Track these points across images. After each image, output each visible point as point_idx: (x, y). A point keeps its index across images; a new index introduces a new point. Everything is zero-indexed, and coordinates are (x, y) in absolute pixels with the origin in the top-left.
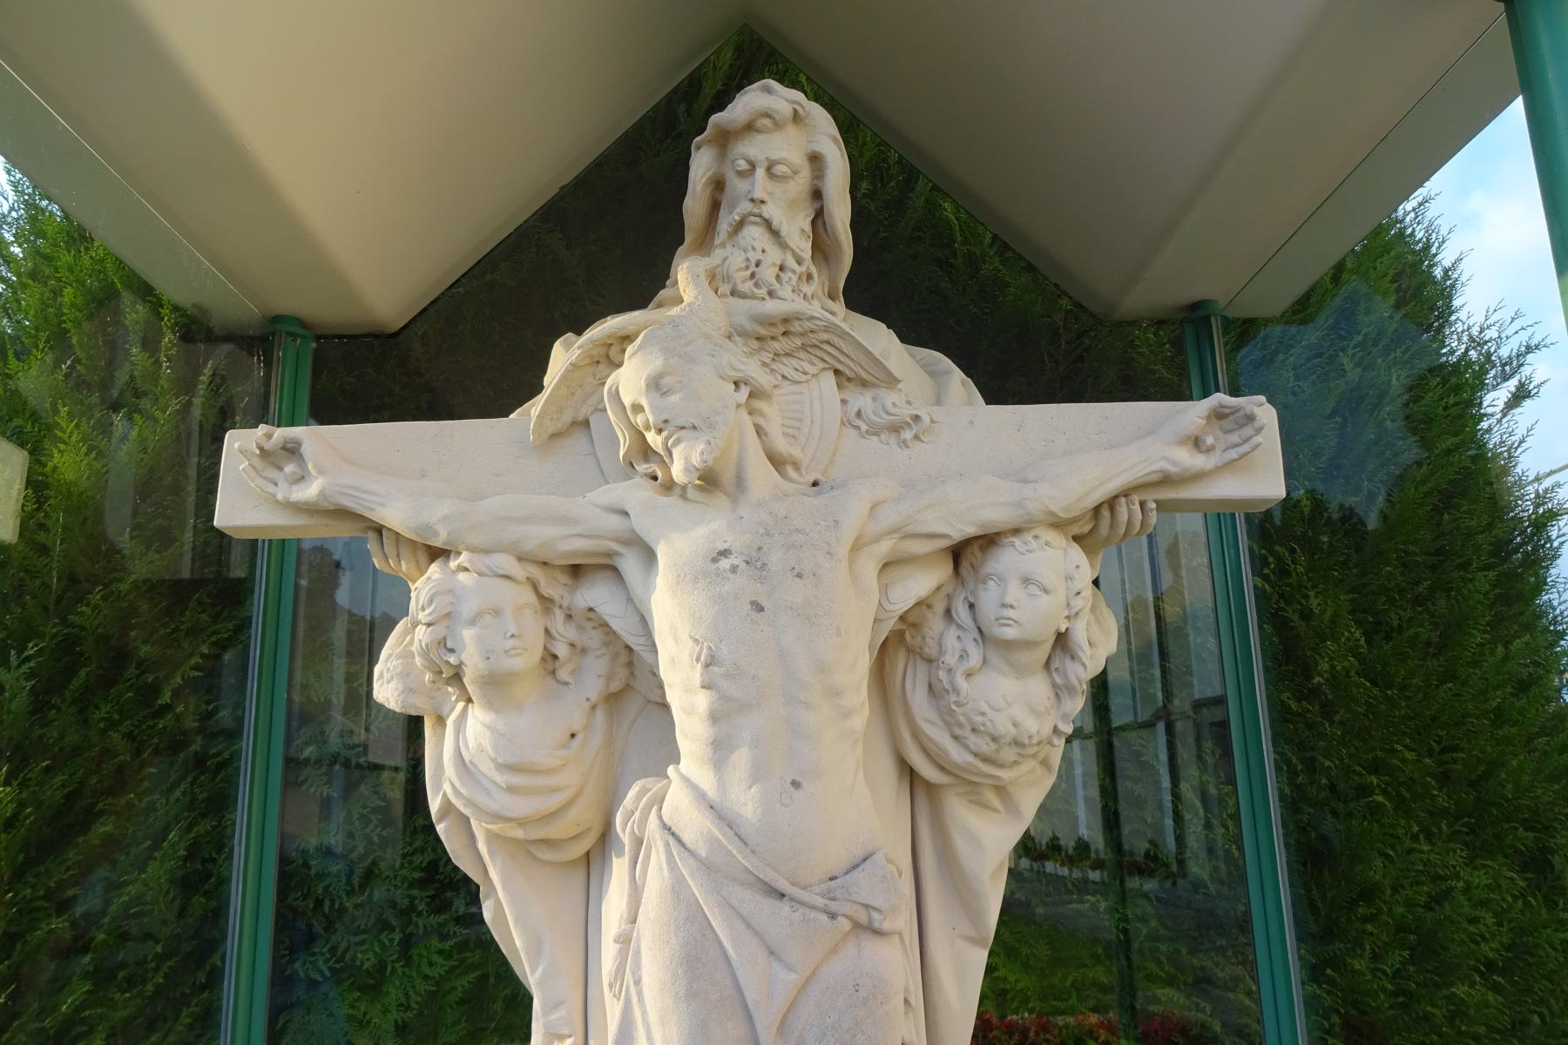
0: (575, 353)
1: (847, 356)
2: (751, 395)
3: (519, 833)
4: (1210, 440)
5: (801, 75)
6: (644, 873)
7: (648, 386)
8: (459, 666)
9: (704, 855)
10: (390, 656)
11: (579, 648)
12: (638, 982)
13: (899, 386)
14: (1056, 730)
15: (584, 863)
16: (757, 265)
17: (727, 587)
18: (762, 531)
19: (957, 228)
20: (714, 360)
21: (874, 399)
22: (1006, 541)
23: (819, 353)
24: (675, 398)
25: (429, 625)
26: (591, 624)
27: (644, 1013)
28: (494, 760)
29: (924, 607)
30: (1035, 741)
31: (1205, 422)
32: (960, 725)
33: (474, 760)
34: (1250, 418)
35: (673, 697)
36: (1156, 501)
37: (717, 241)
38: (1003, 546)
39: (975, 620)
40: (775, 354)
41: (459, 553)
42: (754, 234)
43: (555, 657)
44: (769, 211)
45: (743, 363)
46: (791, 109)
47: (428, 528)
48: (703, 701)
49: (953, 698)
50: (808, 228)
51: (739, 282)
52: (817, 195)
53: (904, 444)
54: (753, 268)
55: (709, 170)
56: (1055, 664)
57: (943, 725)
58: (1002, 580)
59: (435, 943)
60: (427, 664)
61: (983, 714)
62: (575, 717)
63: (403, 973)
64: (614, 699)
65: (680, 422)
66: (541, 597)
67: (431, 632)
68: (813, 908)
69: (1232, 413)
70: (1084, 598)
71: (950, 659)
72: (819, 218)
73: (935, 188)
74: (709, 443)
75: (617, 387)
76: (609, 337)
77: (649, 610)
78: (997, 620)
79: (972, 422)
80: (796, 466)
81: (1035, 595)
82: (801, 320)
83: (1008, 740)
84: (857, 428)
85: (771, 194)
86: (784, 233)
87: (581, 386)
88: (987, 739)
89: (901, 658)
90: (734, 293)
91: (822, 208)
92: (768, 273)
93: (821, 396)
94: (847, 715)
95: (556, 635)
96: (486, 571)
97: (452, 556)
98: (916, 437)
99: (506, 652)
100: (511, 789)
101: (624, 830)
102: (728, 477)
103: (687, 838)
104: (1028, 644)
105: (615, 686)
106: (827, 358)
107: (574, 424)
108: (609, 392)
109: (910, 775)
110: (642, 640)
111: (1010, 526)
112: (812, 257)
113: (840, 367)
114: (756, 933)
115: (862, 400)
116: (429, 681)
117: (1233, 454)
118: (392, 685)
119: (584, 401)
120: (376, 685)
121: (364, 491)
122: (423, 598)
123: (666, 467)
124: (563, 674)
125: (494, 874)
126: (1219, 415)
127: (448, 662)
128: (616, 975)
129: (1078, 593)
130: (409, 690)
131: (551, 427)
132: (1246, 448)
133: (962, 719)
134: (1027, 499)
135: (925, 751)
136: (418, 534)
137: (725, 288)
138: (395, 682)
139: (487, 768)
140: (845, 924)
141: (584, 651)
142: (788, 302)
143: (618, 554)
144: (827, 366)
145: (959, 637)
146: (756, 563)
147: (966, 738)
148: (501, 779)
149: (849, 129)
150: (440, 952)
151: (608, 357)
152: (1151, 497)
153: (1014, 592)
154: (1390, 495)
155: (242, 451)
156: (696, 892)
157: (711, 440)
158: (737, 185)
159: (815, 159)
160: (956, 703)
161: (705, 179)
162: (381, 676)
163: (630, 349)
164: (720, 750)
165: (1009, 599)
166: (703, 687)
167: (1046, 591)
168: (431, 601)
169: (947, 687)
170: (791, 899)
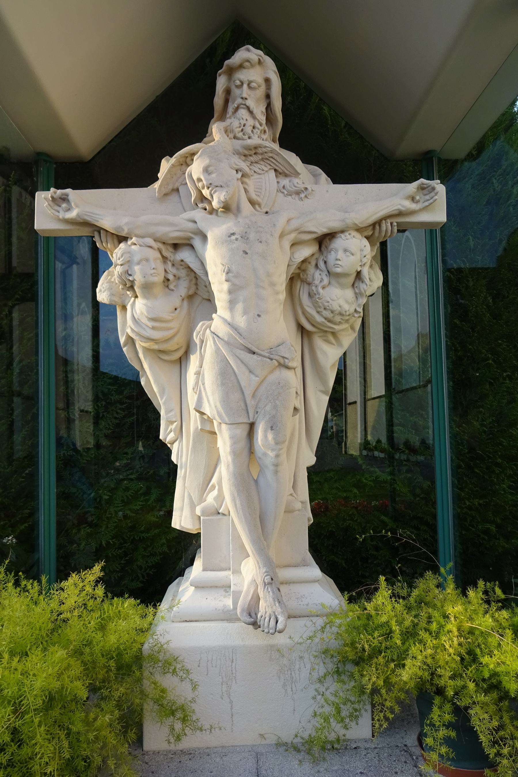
0: (170, 164)
1: (279, 163)
2: (242, 176)
3: (156, 347)
4: (418, 198)
5: (262, 44)
6: (205, 351)
7: (203, 171)
8: (133, 282)
9: (226, 340)
10: (103, 283)
11: (177, 277)
12: (203, 384)
13: (300, 176)
14: (356, 311)
15: (179, 360)
16: (244, 126)
17: (234, 245)
18: (247, 226)
19: (329, 118)
20: (228, 161)
21: (290, 181)
22: (339, 235)
23: (268, 162)
24: (214, 175)
25: (121, 265)
26: (182, 267)
27: (206, 393)
28: (147, 317)
29: (308, 263)
30: (348, 313)
31: (416, 190)
32: (320, 307)
33: (139, 318)
34: (434, 189)
35: (215, 288)
36: (397, 223)
37: (228, 116)
38: (337, 238)
39: (326, 268)
40: (251, 162)
41: (132, 238)
42: (243, 113)
43: (168, 280)
44: (249, 103)
45: (239, 162)
46: (257, 59)
47: (120, 228)
48: (226, 286)
49: (317, 296)
50: (264, 111)
51: (237, 133)
52: (268, 96)
53: (301, 199)
54: (242, 127)
55: (224, 85)
56: (356, 285)
57: (313, 307)
58: (336, 251)
59: (119, 406)
60: (120, 281)
61: (328, 302)
62: (177, 302)
63: (107, 416)
64: (191, 297)
65: (216, 184)
66: (163, 257)
67: (123, 268)
68: (265, 357)
69: (427, 187)
70: (367, 258)
71: (317, 282)
72: (269, 107)
73: (321, 99)
74: (227, 192)
75: (191, 173)
76: (187, 154)
77: (205, 258)
78: (334, 265)
79: (327, 191)
80: (259, 205)
81: (348, 256)
82: (261, 147)
83: (337, 312)
84: (283, 193)
85: (249, 96)
86: (255, 112)
87: (175, 174)
88: (330, 312)
89: (299, 284)
90: (235, 137)
91: (270, 101)
92: (248, 129)
93: (269, 180)
94: (277, 293)
95: (169, 272)
96: (142, 244)
97: (129, 239)
98: (306, 197)
99: (151, 275)
100: (153, 328)
101: (197, 338)
102: (234, 207)
103: (220, 335)
104: (345, 275)
105: (191, 292)
106: (272, 164)
107: (173, 190)
108: (188, 174)
109: (301, 329)
110: (202, 272)
111: (340, 230)
112: (266, 123)
113: (277, 168)
114: (245, 365)
115: (285, 182)
116: (121, 289)
117: (427, 204)
118: (105, 293)
119: (177, 181)
120: (98, 295)
121: (94, 214)
122: (119, 255)
123: (210, 203)
124: (171, 287)
125: (146, 366)
126: (422, 188)
127: (129, 280)
128: (195, 385)
129: (365, 256)
130: (112, 295)
131: (164, 191)
132: (431, 201)
133: (320, 304)
134: (346, 218)
135: (307, 319)
136: (116, 230)
137: (231, 135)
138: (106, 292)
139: (145, 321)
140: (276, 364)
141: (179, 278)
142: (255, 141)
143: (192, 238)
144: (272, 167)
145: (320, 274)
146: (245, 237)
147: (322, 312)
148: (150, 324)
149: (282, 71)
150: (120, 409)
151: (187, 161)
152: (395, 221)
153: (341, 254)
154: (509, 241)
155: (46, 199)
156: (224, 352)
157: (228, 191)
158: (236, 92)
159: (267, 81)
160: (318, 298)
161: (223, 89)
162: (100, 291)
163: (195, 158)
164: (232, 304)
165: (338, 257)
166: (226, 281)
167: (353, 254)
168: (122, 256)
169: (315, 292)
170: (257, 354)
